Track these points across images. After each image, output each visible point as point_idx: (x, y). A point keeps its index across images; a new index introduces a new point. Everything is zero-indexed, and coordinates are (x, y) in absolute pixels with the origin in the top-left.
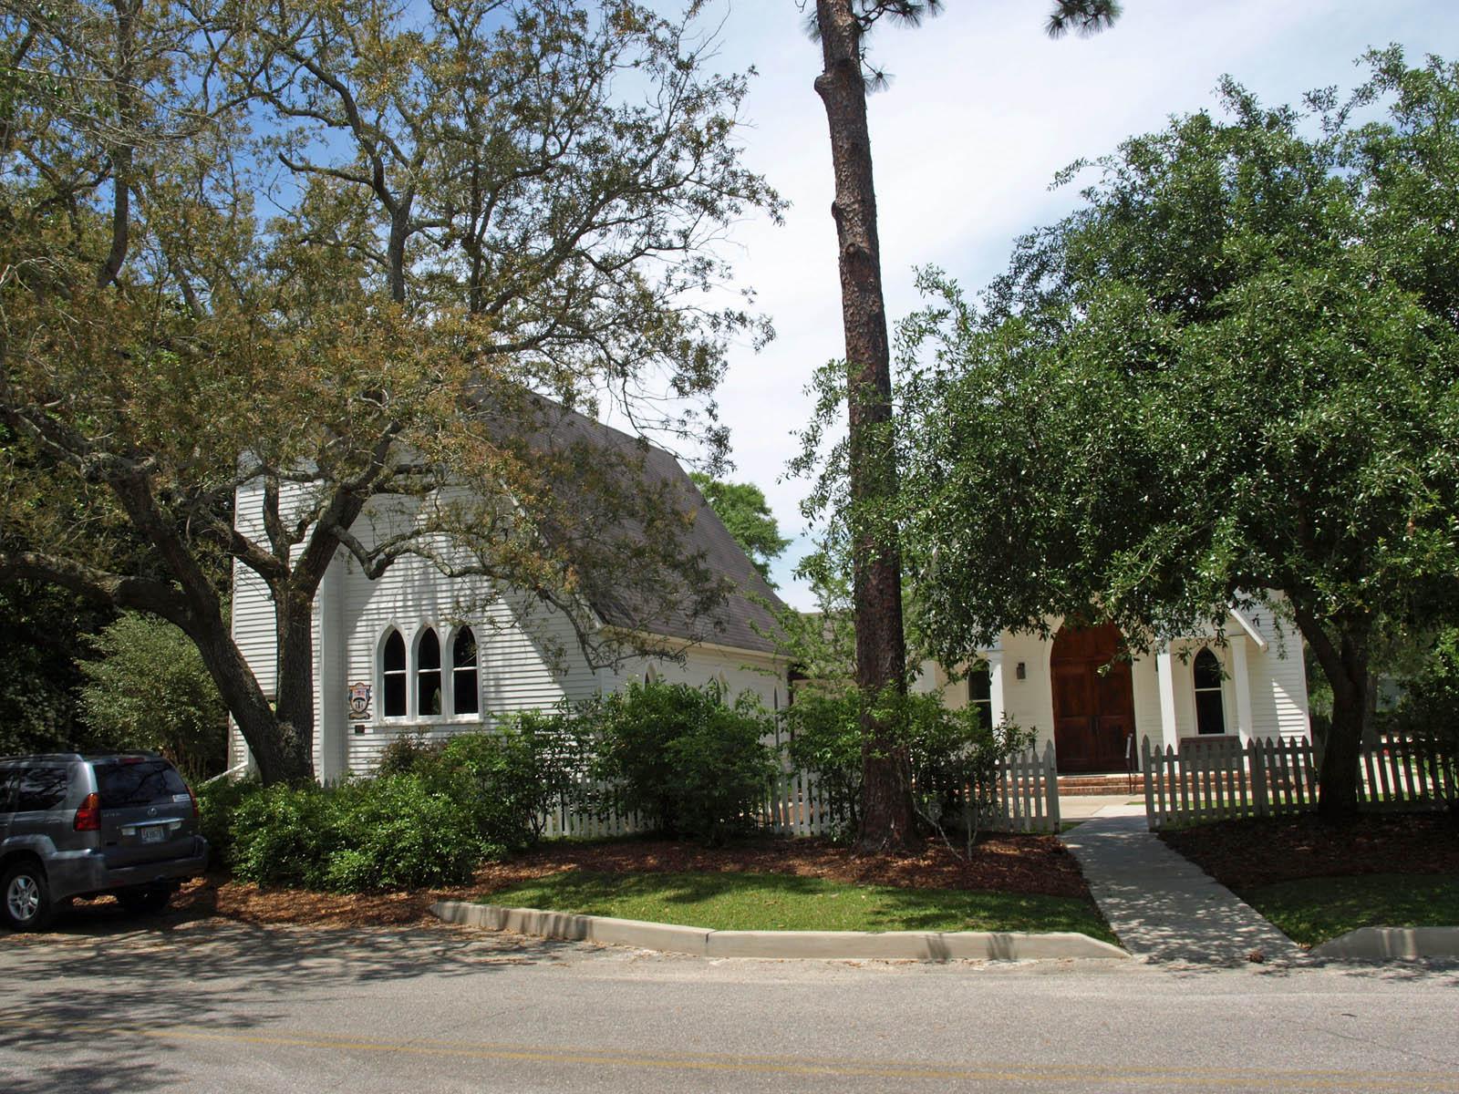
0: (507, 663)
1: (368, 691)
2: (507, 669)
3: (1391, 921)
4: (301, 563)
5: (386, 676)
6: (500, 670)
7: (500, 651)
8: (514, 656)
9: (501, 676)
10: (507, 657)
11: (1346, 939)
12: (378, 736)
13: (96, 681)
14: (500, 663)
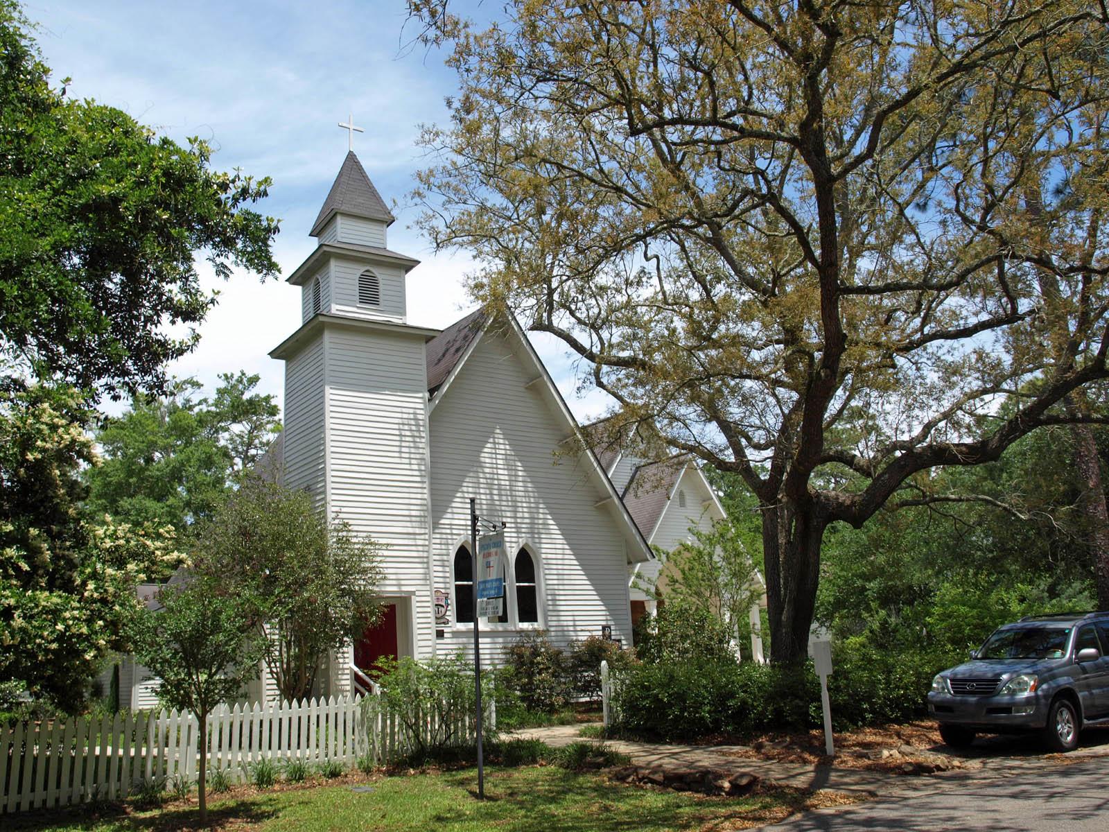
0: (561, 582)
1: (447, 598)
2: (561, 587)
3: (964, 449)
4: (740, 441)
5: (470, 580)
6: (556, 587)
7: (555, 572)
8: (566, 577)
9: (557, 592)
10: (560, 577)
11: (563, 715)
12: (455, 641)
13: (698, 535)
14: (555, 582)
